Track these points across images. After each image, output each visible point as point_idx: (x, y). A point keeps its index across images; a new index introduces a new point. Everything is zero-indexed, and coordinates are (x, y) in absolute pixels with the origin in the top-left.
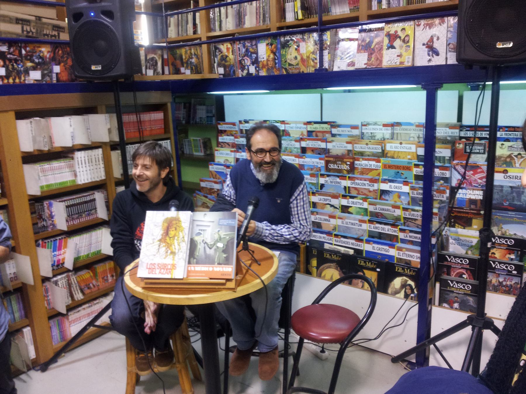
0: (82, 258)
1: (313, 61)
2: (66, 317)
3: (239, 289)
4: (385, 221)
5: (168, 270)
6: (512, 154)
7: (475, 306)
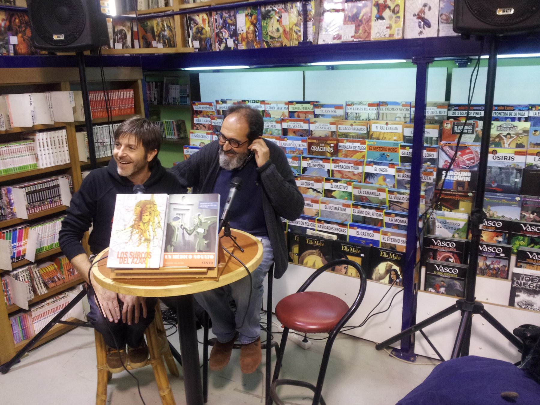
0: (44, 249)
1: (296, 33)
2: (28, 313)
3: (222, 278)
4: (369, 205)
5: (142, 259)
6: (501, 133)
7: (462, 290)
